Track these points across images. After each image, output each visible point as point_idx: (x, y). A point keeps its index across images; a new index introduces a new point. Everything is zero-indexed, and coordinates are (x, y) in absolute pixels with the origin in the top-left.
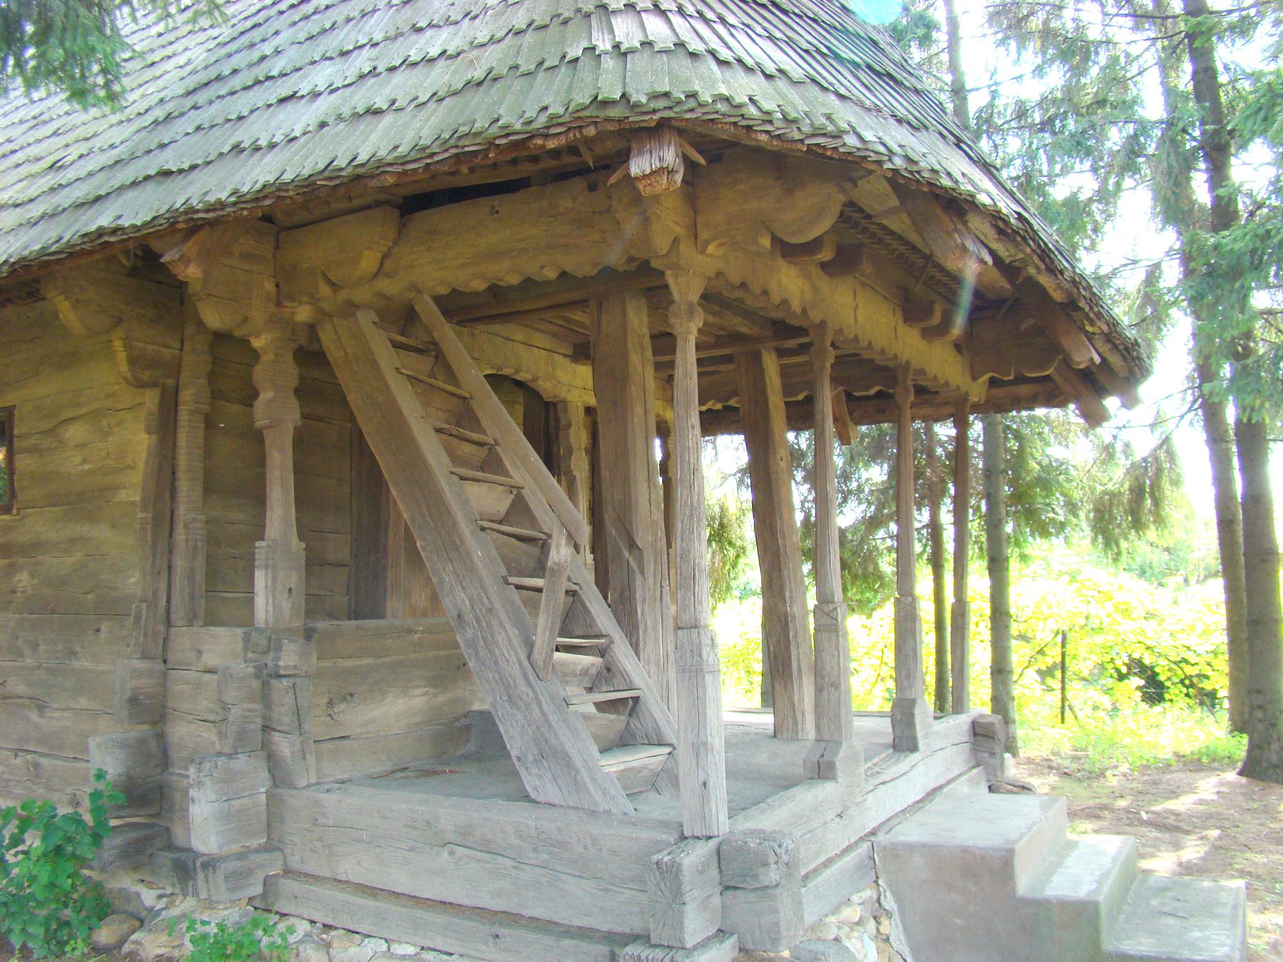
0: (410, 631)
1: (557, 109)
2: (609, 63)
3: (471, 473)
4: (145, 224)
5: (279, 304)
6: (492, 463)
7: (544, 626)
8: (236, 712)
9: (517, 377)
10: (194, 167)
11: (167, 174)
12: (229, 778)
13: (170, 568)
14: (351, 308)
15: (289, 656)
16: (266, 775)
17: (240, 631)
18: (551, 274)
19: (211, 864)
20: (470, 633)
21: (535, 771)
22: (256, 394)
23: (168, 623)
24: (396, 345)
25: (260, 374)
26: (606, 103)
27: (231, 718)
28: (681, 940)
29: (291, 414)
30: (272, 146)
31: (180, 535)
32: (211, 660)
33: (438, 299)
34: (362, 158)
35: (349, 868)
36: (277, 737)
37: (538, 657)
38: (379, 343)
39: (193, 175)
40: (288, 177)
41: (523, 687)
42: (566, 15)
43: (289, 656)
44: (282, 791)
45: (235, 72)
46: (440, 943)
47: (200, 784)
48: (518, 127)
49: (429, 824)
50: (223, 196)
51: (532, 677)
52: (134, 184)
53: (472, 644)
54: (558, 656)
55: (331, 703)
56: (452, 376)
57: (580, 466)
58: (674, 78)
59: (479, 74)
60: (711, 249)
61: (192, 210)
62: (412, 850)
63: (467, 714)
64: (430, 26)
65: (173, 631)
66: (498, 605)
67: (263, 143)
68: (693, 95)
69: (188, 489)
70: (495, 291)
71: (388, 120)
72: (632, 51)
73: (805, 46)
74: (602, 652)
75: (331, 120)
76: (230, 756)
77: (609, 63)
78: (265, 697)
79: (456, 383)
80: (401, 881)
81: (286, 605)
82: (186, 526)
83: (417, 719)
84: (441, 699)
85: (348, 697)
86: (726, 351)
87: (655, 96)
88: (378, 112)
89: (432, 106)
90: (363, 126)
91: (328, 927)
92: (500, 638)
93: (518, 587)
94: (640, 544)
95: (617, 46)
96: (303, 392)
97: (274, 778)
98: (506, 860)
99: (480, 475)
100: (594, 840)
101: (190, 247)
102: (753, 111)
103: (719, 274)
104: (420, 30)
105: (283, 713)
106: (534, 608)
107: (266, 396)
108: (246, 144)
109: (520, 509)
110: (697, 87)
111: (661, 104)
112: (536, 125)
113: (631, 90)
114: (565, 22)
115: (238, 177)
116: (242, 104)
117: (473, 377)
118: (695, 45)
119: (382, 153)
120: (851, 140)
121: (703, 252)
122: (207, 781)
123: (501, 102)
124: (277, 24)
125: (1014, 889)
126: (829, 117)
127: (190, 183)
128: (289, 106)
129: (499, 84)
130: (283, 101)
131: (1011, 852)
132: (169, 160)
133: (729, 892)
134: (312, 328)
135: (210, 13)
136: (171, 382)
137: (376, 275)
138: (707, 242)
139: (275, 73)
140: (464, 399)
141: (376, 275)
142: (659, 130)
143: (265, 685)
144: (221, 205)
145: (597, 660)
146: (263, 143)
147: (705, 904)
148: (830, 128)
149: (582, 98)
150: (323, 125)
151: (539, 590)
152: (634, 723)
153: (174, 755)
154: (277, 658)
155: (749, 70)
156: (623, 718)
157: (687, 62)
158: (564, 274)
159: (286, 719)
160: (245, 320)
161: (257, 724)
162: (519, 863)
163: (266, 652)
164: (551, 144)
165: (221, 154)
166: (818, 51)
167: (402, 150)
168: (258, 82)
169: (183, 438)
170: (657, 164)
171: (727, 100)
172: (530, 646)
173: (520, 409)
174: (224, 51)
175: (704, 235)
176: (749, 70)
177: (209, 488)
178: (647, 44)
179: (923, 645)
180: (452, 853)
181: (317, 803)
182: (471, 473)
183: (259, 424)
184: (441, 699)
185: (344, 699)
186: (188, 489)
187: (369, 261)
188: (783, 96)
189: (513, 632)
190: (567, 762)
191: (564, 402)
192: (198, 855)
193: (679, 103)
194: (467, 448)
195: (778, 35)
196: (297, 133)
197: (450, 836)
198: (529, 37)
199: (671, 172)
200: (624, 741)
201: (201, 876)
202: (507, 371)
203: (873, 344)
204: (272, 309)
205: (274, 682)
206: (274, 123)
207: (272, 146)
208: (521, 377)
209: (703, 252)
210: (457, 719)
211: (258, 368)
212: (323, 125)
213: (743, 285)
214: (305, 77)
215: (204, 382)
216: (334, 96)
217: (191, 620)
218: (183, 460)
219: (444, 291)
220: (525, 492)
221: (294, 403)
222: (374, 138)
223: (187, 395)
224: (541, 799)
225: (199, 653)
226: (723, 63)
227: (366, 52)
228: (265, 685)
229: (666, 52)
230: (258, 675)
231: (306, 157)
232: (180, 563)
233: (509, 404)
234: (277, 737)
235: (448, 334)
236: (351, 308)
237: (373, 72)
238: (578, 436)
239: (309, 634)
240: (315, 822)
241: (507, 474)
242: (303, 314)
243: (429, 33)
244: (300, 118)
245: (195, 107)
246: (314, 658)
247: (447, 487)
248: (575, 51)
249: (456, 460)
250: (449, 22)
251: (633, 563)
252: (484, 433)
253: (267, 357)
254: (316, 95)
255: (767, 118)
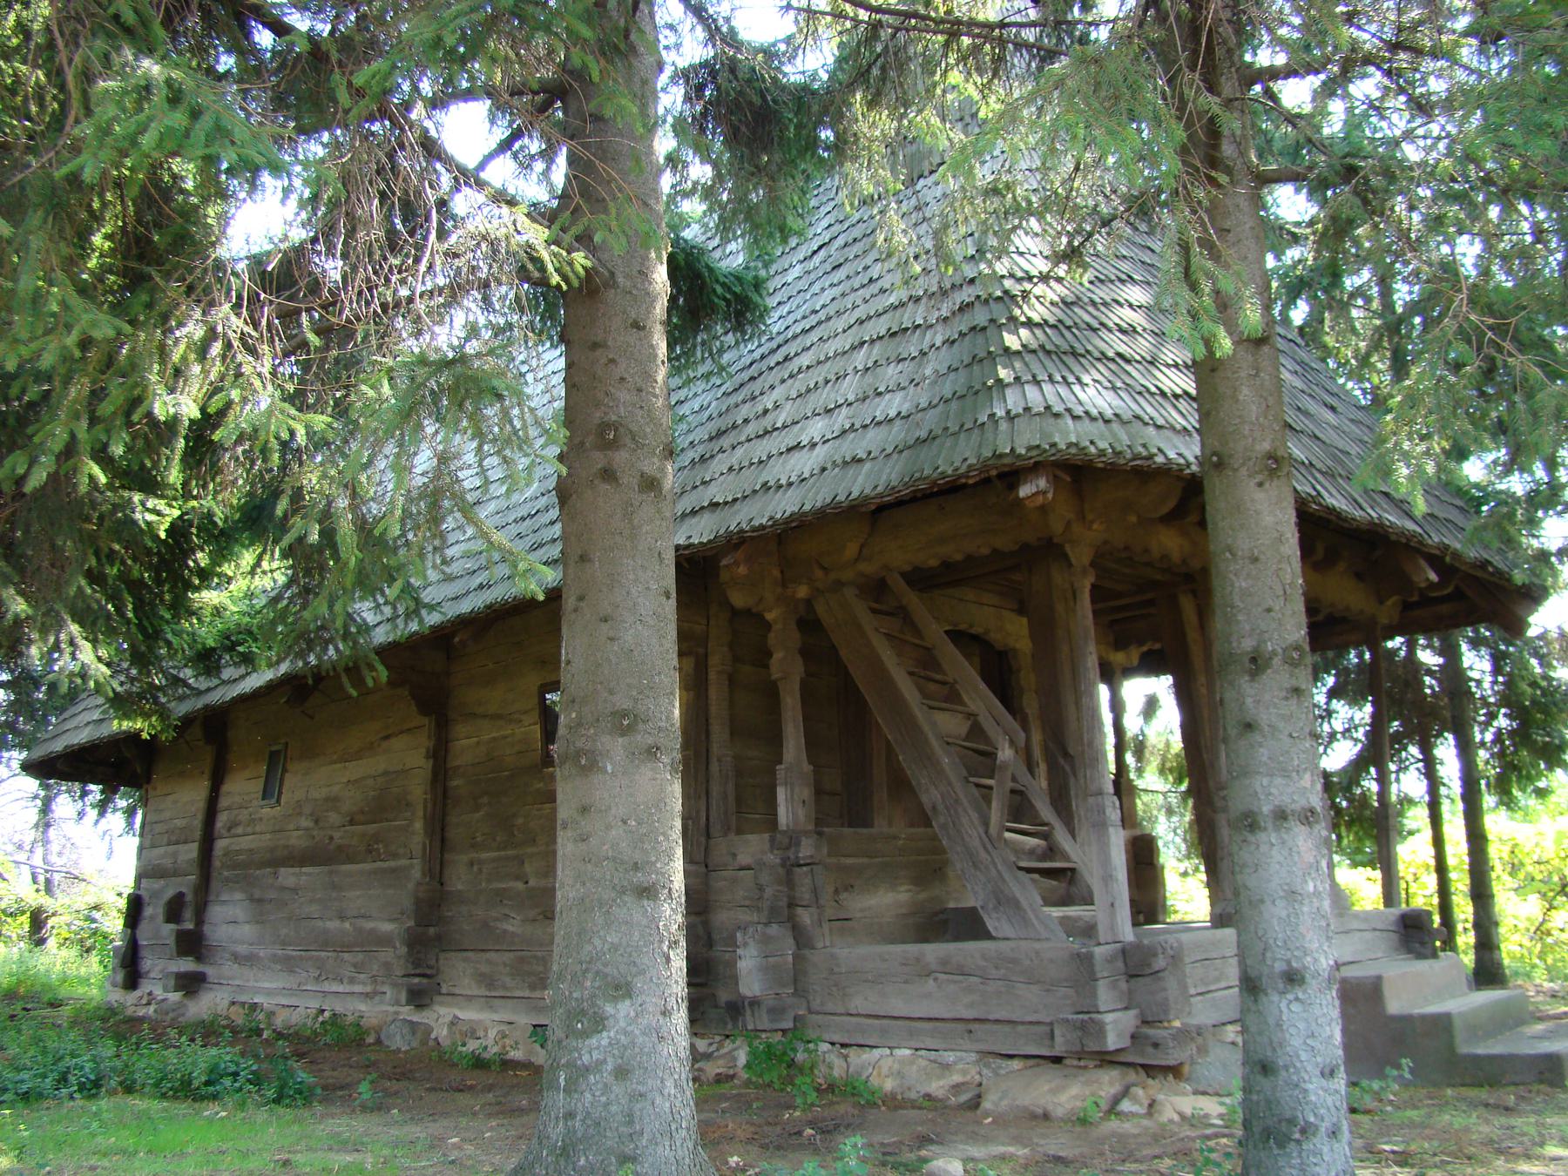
0: (895, 838)
1: (972, 461)
2: (1003, 426)
3: (936, 704)
4: (710, 541)
5: (784, 585)
6: (951, 697)
7: (996, 812)
8: (769, 892)
9: (973, 631)
10: (735, 500)
11: (714, 505)
12: (766, 940)
13: (707, 793)
14: (839, 585)
15: (806, 850)
16: (791, 941)
17: (766, 836)
18: (985, 551)
19: (755, 1003)
20: (942, 819)
21: (994, 915)
22: (770, 655)
23: (708, 836)
24: (874, 611)
25: (772, 638)
26: (1001, 456)
27: (766, 896)
28: (1096, 1006)
29: (798, 669)
30: (790, 484)
31: (714, 767)
32: (744, 859)
33: (903, 575)
34: (855, 494)
35: (858, 1003)
36: (800, 910)
37: (993, 830)
38: (861, 610)
39: (737, 506)
40: (807, 507)
41: (983, 855)
42: (977, 387)
43: (806, 850)
44: (806, 952)
45: (746, 421)
46: (930, 1043)
47: (745, 944)
48: (950, 472)
49: (918, 960)
50: (764, 521)
51: (989, 846)
52: (694, 513)
53: (944, 827)
54: (1008, 835)
55: (836, 892)
56: (918, 633)
57: (1031, 704)
58: (1044, 434)
59: (923, 434)
60: (1095, 526)
61: (742, 531)
62: (906, 982)
63: (944, 911)
64: (888, 391)
65: (712, 842)
66: (962, 796)
67: (783, 482)
68: (1053, 445)
69: (719, 733)
70: (947, 565)
71: (868, 466)
72: (1018, 415)
73: (1139, 388)
74: (1045, 836)
75: (829, 466)
76: (766, 924)
77: (1003, 426)
78: (789, 882)
79: (921, 637)
80: (898, 1007)
81: (801, 812)
82: (719, 760)
83: (904, 911)
84: (923, 896)
85: (849, 888)
86: (1149, 596)
87: (1030, 449)
88: (860, 461)
89: (895, 456)
90: (851, 471)
91: (843, 1045)
92: (965, 820)
93: (977, 785)
94: (1071, 752)
95: (1008, 412)
96: (806, 653)
97: (798, 944)
98: (972, 979)
99: (944, 705)
100: (1037, 953)
101: (740, 554)
102: (1093, 450)
103: (1105, 542)
104: (880, 394)
105: (804, 892)
106: (988, 800)
107: (778, 655)
108: (771, 483)
109: (976, 731)
110: (1057, 440)
111: (1034, 453)
112: (961, 471)
113: (1016, 446)
114: (976, 393)
115: (770, 508)
116: (761, 449)
117: (935, 632)
118: (1058, 408)
119: (867, 491)
120: (1160, 459)
121: (1090, 529)
122: (751, 941)
123: (938, 456)
124: (771, 378)
125: (1384, 1009)
126: (1144, 446)
127: (736, 513)
128: (796, 455)
129: (938, 441)
130: (789, 450)
131: (1379, 978)
132: (716, 493)
133: (1133, 981)
134: (808, 602)
135: (719, 373)
136: (701, 651)
137: (857, 560)
138: (1092, 522)
139: (779, 425)
140: (928, 649)
141: (857, 560)
142: (1035, 468)
143: (789, 873)
144: (762, 527)
145: (1042, 843)
146: (783, 482)
147: (1114, 986)
148: (1145, 453)
149: (987, 453)
150: (824, 469)
151: (990, 788)
152: (1074, 889)
153: (716, 937)
154: (797, 852)
155: (1093, 419)
156: (1064, 885)
157: (1052, 420)
158: (995, 551)
159: (807, 896)
160: (761, 600)
161: (783, 903)
162: (985, 979)
163: (788, 848)
164: (971, 481)
165: (755, 492)
166: (1148, 390)
167: (880, 489)
168: (766, 432)
169: (713, 693)
170: (1034, 490)
171: (1076, 445)
172: (986, 824)
173: (977, 660)
174: (732, 400)
175: (1090, 517)
176: (1093, 419)
177: (735, 732)
178: (1027, 409)
179: (1502, 930)
180: (935, 979)
181: (833, 956)
182: (936, 704)
183: (775, 676)
184: (923, 896)
185: (846, 890)
186: (719, 733)
187: (851, 550)
188: (1114, 435)
189: (974, 816)
190: (1016, 904)
191: (1014, 650)
192: (744, 998)
193: (1045, 451)
194: (932, 687)
195: (1119, 384)
196: (806, 475)
197: (934, 967)
198: (954, 405)
199: (1044, 493)
200: (1065, 901)
201: (748, 1012)
202: (963, 627)
203: (574, 647)
204: (779, 590)
205: (797, 870)
206: (788, 467)
207: (790, 484)
208: (977, 630)
209: (1090, 529)
210: (936, 914)
211: (772, 635)
212: (824, 469)
213: (1126, 548)
214: (803, 429)
215: (725, 649)
216: (827, 445)
217: (727, 830)
218: (713, 710)
219: (907, 568)
220: (981, 719)
221: (799, 661)
222: (860, 479)
223: (715, 661)
224: (1000, 935)
225: (734, 855)
226: (1075, 418)
227: (844, 410)
228: (789, 873)
229: (1038, 414)
230: (783, 865)
231: (817, 493)
232: (715, 789)
233: (967, 656)
234: (800, 910)
235: (912, 600)
236: (839, 585)
237: (852, 428)
238: (1028, 679)
239: (820, 834)
240: (831, 972)
241: (962, 703)
242: (802, 592)
243: (888, 396)
244: (804, 463)
245: (722, 451)
246: (825, 850)
247: (919, 713)
248: (983, 418)
249: (925, 695)
250: (899, 387)
251: (1067, 768)
252: (945, 674)
253: (777, 627)
254: (813, 445)
255: (1102, 453)
